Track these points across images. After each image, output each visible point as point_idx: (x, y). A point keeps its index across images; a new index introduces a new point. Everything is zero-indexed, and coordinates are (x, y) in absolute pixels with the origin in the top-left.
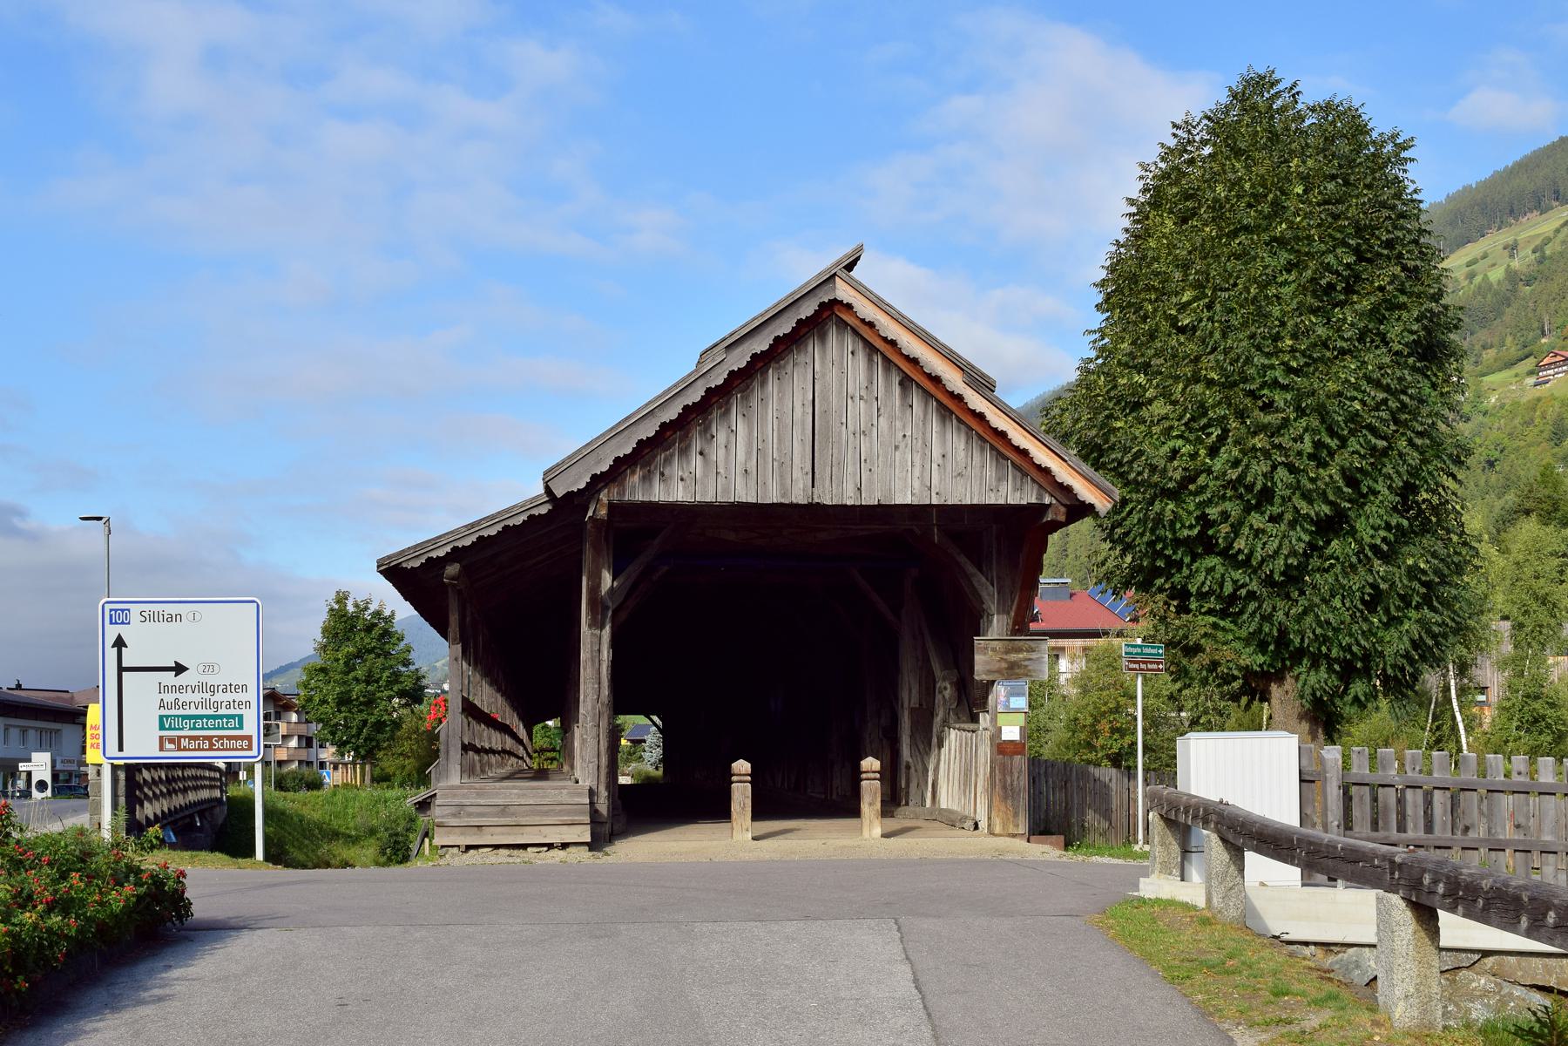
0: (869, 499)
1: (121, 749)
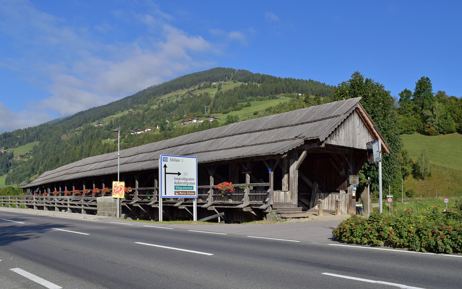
0: (360, 148)
1: (166, 194)
